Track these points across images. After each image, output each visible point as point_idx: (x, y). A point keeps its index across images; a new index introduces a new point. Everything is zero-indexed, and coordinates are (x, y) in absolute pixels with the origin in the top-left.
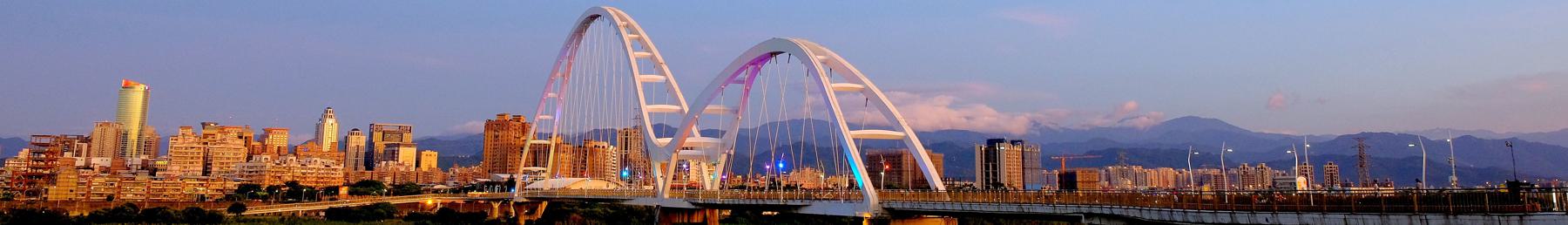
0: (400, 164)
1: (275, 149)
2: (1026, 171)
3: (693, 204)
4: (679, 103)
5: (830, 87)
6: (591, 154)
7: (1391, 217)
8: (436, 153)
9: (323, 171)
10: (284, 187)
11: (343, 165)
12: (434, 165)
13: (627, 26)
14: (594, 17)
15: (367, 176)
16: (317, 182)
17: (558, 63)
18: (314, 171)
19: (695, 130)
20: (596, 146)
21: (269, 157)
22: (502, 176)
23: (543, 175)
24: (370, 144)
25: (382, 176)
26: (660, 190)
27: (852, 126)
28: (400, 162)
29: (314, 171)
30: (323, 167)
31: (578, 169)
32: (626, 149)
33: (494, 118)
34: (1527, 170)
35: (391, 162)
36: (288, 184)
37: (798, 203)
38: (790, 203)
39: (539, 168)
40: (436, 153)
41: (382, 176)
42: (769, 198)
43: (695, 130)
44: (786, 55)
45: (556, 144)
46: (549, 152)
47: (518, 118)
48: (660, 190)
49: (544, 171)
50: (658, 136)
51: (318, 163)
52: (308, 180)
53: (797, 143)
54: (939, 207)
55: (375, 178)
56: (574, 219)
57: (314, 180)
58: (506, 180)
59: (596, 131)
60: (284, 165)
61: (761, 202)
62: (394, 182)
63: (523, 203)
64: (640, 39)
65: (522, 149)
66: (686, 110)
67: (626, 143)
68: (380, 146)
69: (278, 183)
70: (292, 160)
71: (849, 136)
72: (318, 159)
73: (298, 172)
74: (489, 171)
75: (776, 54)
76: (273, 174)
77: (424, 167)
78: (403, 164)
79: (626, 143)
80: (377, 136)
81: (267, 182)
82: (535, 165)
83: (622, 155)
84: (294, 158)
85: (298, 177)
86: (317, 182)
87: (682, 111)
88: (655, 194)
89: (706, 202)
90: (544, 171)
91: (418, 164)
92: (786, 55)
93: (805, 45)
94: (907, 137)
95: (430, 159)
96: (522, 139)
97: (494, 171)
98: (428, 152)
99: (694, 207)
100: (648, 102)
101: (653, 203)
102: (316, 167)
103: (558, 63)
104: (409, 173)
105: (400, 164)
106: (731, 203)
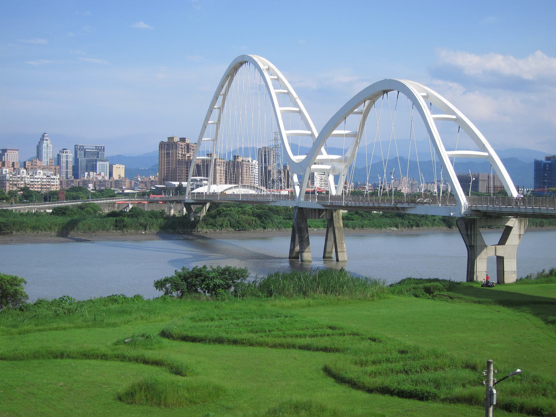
0: (98, 175)
1: (11, 164)
3: (323, 206)
4: (309, 128)
5: (430, 117)
7: (367, 206)
8: (124, 166)
9: (45, 180)
10: (20, 191)
11: (59, 175)
12: (123, 175)
13: (268, 69)
14: (241, 64)
15: (75, 184)
16: (42, 188)
17: (216, 98)
18: (39, 180)
19: (323, 149)
20: (243, 161)
21: (7, 170)
22: (174, 183)
24: (76, 160)
25: (86, 183)
26: (298, 195)
27: (447, 149)
28: (98, 173)
29: (39, 180)
30: (45, 177)
32: (265, 162)
33: (166, 140)
35: (91, 173)
36: (22, 189)
37: (406, 205)
38: (399, 205)
39: (202, 178)
40: (124, 166)
41: (86, 183)
42: (383, 201)
43: (323, 149)
47: (183, 140)
48: (298, 195)
50: (295, 154)
51: (40, 174)
52: (35, 186)
53: (241, 147)
54: (515, 210)
55: (81, 185)
57: (39, 186)
58: (176, 186)
59: (246, 149)
60: (18, 176)
61: (371, 205)
62: (95, 188)
64: (278, 79)
66: (316, 135)
67: (265, 159)
68: (82, 160)
69: (15, 188)
70: (23, 172)
71: (445, 155)
72: (41, 171)
73: (28, 181)
74: (164, 179)
75: (386, 92)
76: (11, 183)
77: (115, 177)
79: (265, 159)
80: (80, 153)
81: (7, 188)
83: (262, 168)
84: (25, 171)
85: (28, 184)
86: (42, 188)
87: (312, 135)
88: (292, 195)
89: (243, 200)
91: (111, 174)
92: (396, 92)
93: (256, 58)
94: (490, 157)
95: (119, 171)
98: (118, 165)
99: (323, 208)
100: (286, 129)
101: (291, 204)
102: (40, 176)
103: (216, 98)
104: (105, 181)
106: (353, 205)
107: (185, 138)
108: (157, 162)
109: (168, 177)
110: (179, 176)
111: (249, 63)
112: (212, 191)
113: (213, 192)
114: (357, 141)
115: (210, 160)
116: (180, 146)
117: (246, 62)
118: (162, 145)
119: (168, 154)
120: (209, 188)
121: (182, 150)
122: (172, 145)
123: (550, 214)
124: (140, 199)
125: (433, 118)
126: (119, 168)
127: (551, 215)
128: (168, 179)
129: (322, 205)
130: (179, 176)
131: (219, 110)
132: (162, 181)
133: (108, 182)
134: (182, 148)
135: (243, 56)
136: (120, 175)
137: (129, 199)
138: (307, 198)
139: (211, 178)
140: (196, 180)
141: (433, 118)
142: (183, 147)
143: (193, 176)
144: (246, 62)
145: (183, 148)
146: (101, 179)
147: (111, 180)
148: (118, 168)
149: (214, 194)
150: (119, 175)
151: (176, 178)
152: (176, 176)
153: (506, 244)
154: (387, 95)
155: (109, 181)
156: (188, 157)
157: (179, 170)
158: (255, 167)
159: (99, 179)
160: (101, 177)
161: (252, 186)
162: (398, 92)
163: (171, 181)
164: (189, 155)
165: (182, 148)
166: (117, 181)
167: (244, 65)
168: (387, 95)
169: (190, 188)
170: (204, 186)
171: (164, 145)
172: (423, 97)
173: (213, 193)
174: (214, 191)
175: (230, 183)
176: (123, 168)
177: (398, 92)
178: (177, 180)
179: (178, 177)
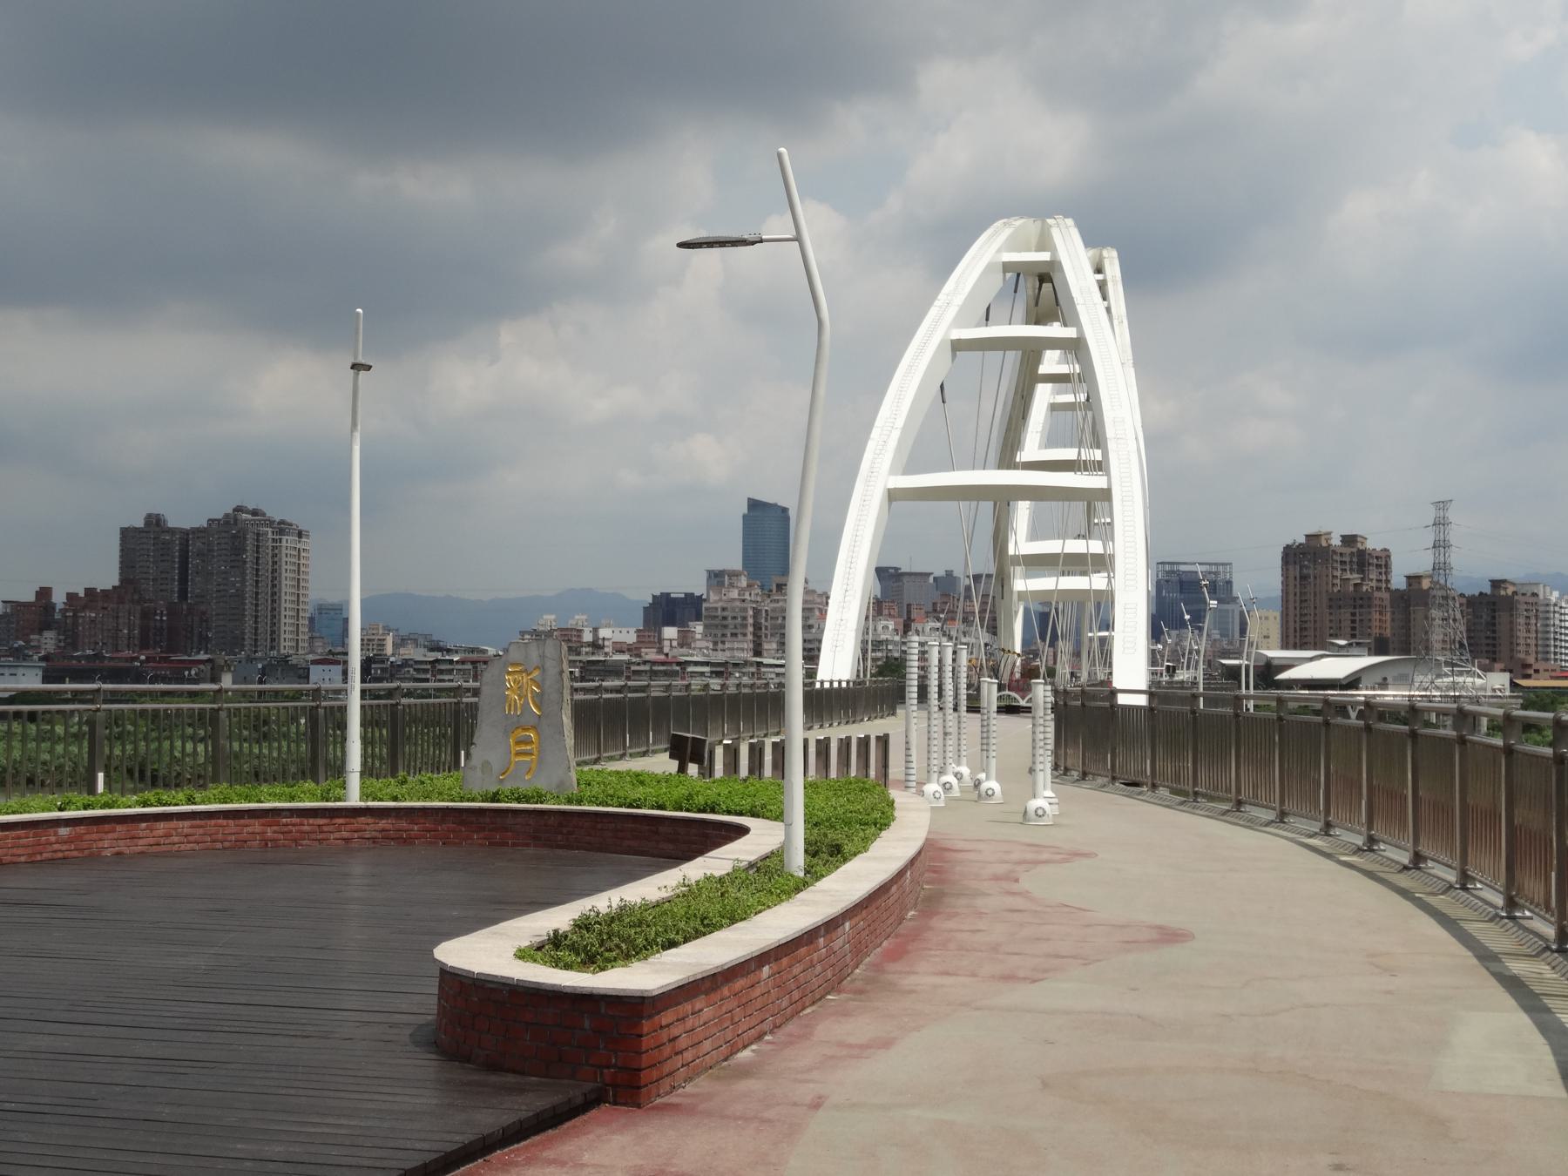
116: (1338, 558)
118: (1291, 555)
134: (1343, 563)
156: (1355, 585)
165: (1343, 563)
176: (1275, 618)
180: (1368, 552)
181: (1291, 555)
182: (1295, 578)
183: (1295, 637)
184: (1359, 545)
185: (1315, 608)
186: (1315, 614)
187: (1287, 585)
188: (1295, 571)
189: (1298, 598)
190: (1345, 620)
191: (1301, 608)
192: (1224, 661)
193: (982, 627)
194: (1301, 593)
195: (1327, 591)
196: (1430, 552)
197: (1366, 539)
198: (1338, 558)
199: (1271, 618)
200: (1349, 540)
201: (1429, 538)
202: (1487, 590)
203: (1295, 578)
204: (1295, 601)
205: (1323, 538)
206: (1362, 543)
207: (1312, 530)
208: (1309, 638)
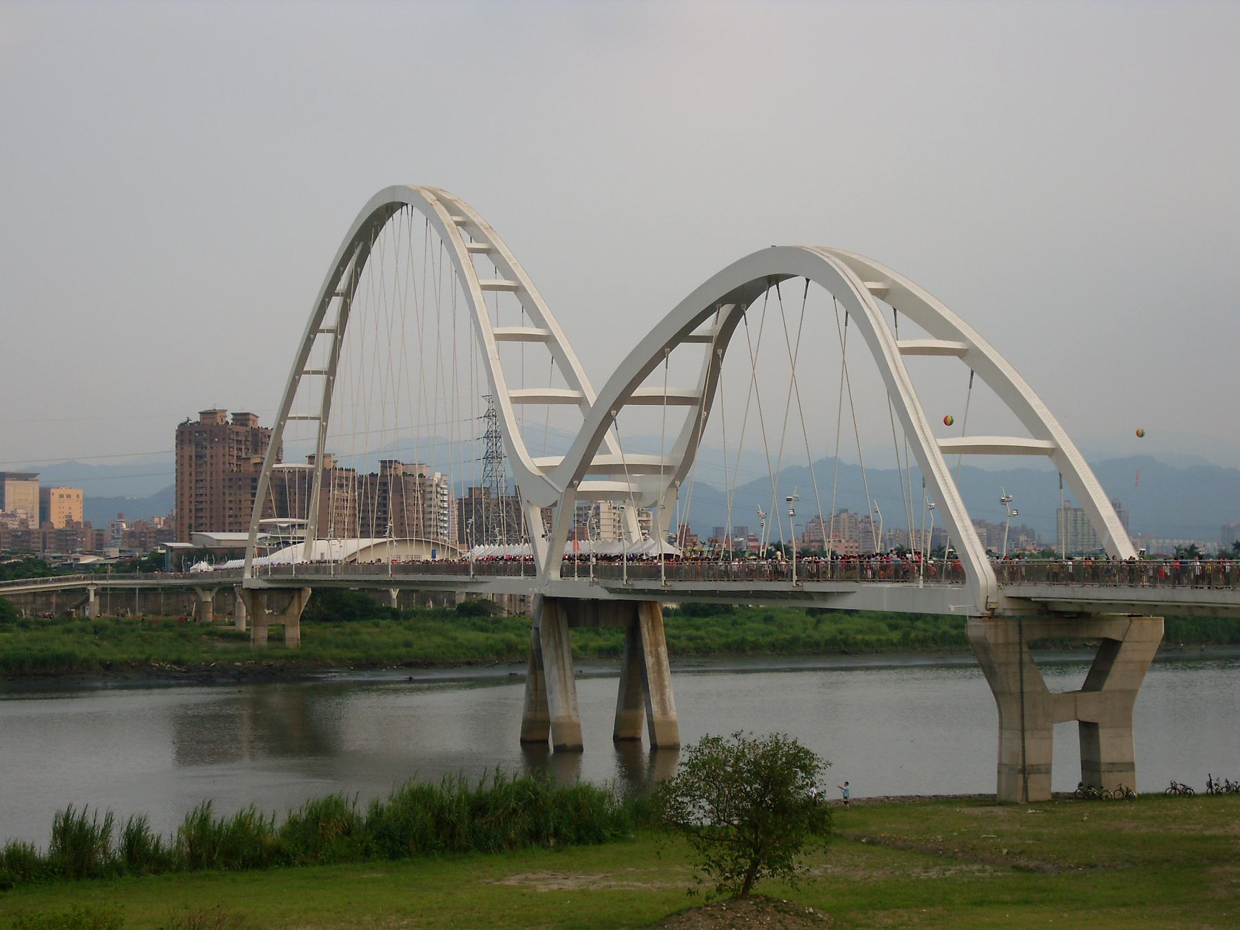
0: (7, 515)
2: (1018, 689)
6: (398, 490)
23: (300, 533)
28: (8, 510)
31: (373, 523)
33: (196, 418)
34: (1087, 609)
44: (801, 280)
45: (324, 469)
46: (310, 487)
49: (301, 526)
50: (533, 453)
56: (666, 613)
63: (261, 590)
65: (255, 480)
75: (774, 280)
78: (13, 515)
82: (283, 514)
87: (581, 401)
90: (301, 526)
96: (253, 461)
97: (200, 527)
104: (29, 533)
105: (7, 515)
107: (248, 414)
108: (171, 480)
109: (200, 521)
110: (230, 516)
111: (410, 206)
112: (316, 557)
113: (319, 558)
114: (700, 415)
115: (311, 472)
116: (233, 436)
117: (402, 204)
118: (186, 433)
119: (199, 457)
120: (308, 550)
121: (240, 447)
122: (211, 431)
123: (1172, 604)
124: (65, 582)
125: (495, 335)
126: (69, 496)
127: (1133, 602)
128: (202, 524)
129: (607, 588)
130: (230, 516)
131: (331, 336)
132: (186, 531)
133: (36, 535)
134: (239, 442)
135: (393, 189)
136: (71, 516)
137: (90, 582)
138: (566, 572)
139: (311, 522)
140: (274, 526)
141: (495, 335)
142: (243, 439)
143: (263, 517)
144: (402, 204)
145: (241, 441)
146: (15, 526)
147: (43, 530)
148: (65, 496)
149: (320, 566)
150: (66, 516)
151: (224, 524)
152: (224, 516)
153: (1106, 687)
154: (778, 288)
155: (39, 533)
156: (256, 464)
157: (231, 501)
158: (439, 489)
159: (10, 526)
160: (16, 523)
161: (438, 544)
162: (808, 280)
163: (211, 531)
164: (258, 460)
165: (239, 442)
166: (60, 532)
167: (397, 215)
168: (778, 288)
169: (256, 549)
170: (294, 543)
171: (190, 432)
172: (874, 292)
173: (318, 562)
174: (322, 554)
175: (365, 534)
176: (78, 496)
177: (808, 280)
178: (227, 528)
179: (228, 520)
180: (261, 430)
181: (186, 433)
182: (191, 456)
183: (190, 517)
184: (251, 424)
185: (212, 488)
186: (212, 495)
187: (182, 465)
188: (190, 450)
189: (193, 477)
190: (245, 500)
191: (196, 488)
192: (169, 544)
193: (728, 534)
194: (196, 473)
195: (224, 472)
196: (482, 463)
197: (258, 417)
198: (233, 436)
199: (74, 497)
200: (242, 418)
201: (482, 448)
202: (377, 470)
203: (191, 456)
204: (190, 481)
205: (218, 415)
206: (254, 421)
207: (208, 407)
208: (204, 519)
